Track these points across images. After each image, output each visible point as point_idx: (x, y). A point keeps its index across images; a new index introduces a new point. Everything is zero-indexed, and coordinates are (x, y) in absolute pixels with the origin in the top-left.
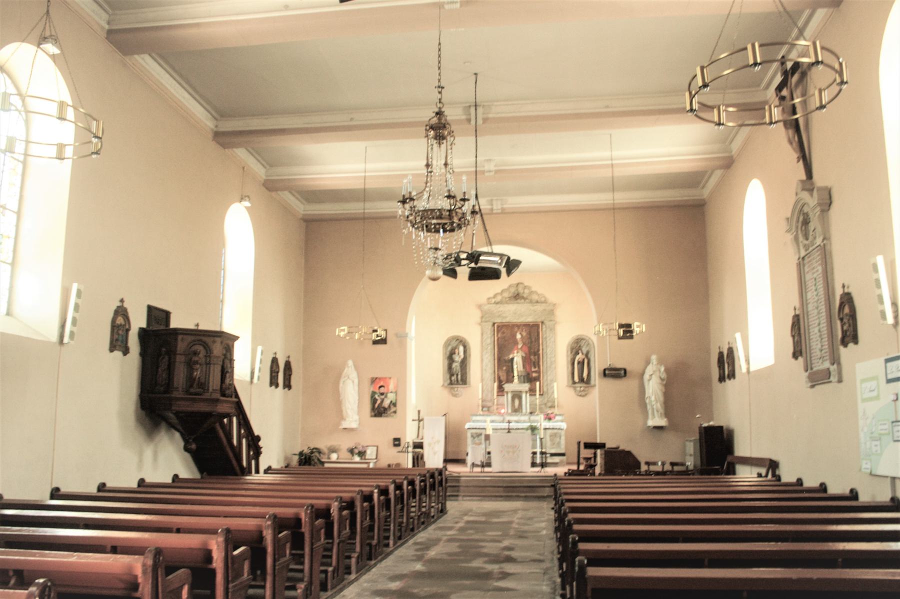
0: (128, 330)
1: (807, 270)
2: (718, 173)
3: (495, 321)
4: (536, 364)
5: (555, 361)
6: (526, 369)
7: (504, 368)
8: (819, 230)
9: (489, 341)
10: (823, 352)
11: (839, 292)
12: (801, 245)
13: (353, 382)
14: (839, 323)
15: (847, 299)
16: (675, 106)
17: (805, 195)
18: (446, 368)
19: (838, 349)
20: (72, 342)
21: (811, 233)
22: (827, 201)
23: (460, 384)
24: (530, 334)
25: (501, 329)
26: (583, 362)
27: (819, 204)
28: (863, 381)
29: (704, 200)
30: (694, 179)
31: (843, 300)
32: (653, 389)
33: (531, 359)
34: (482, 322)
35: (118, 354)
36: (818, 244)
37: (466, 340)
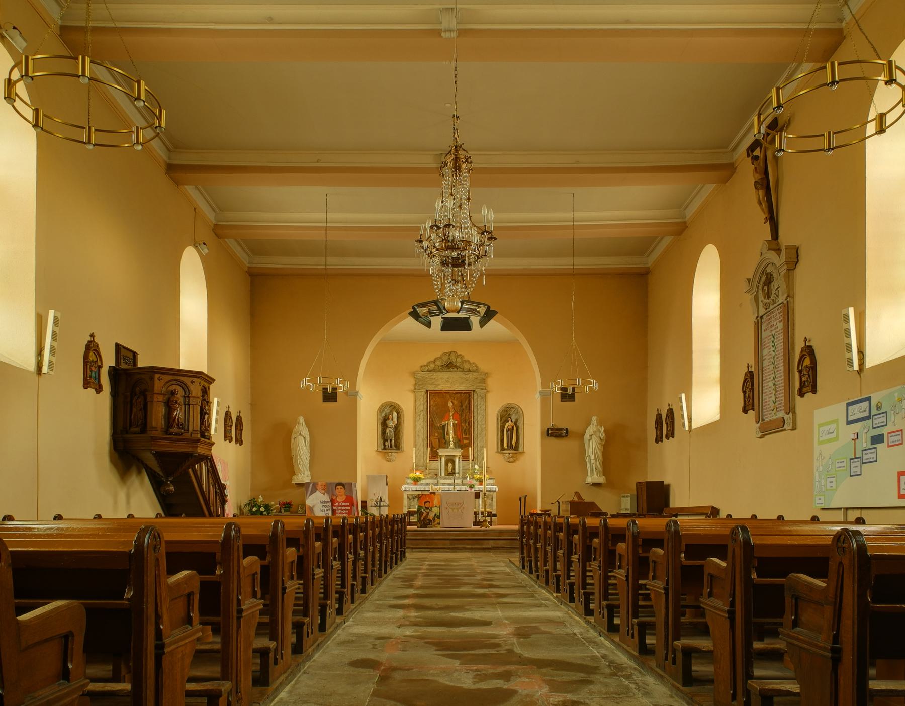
0: (100, 367)
1: (764, 328)
2: (668, 240)
8: (783, 287)
9: (422, 408)
10: (776, 404)
11: (799, 346)
12: (761, 304)
13: (305, 438)
14: (797, 375)
15: (809, 351)
16: (644, 165)
17: (772, 256)
19: (794, 400)
20: (51, 372)
21: (774, 292)
22: (794, 258)
23: (394, 450)
26: (513, 429)
27: (787, 263)
28: (820, 425)
29: (649, 268)
30: (644, 245)
31: (804, 353)
32: (593, 447)
34: (415, 389)
35: (91, 391)
36: (780, 302)
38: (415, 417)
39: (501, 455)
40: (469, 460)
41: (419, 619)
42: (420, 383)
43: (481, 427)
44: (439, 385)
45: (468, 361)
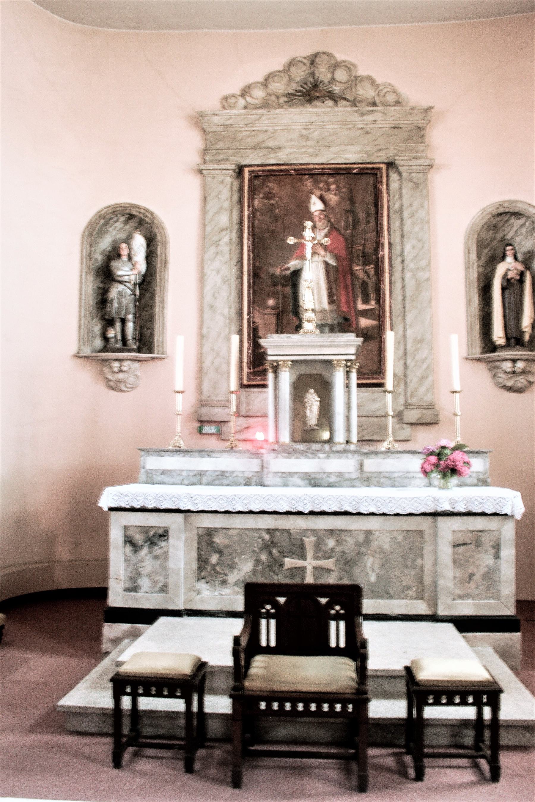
3: (245, 163)
4: (371, 288)
5: (428, 280)
6: (339, 306)
7: (271, 302)
9: (224, 220)
18: (91, 300)
23: (131, 351)
24: (351, 200)
25: (263, 184)
26: (521, 281)
33: (353, 274)
34: (205, 162)
37: (153, 217)
38: (203, 249)
39: (482, 366)
40: (381, 385)
41: (296, 531)
42: (221, 145)
43: (414, 276)
44: (279, 148)
45: (372, 81)
